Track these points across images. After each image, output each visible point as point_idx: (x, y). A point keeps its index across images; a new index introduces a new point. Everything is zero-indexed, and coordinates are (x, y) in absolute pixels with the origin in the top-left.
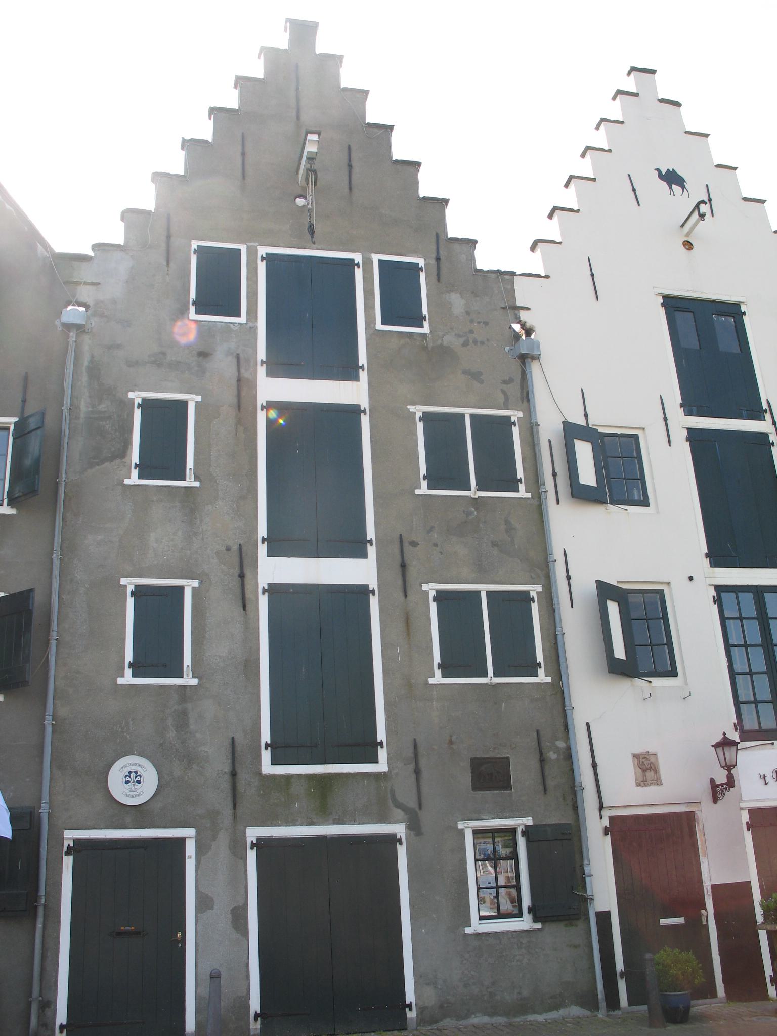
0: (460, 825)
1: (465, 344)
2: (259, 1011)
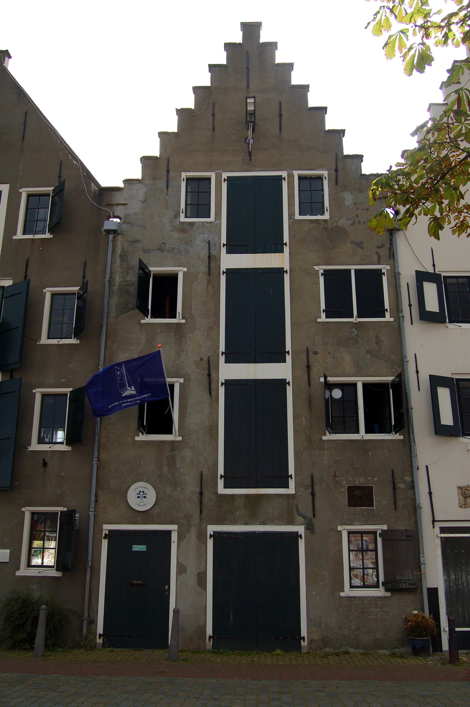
0: (339, 528)
1: (353, 224)
2: (211, 635)
